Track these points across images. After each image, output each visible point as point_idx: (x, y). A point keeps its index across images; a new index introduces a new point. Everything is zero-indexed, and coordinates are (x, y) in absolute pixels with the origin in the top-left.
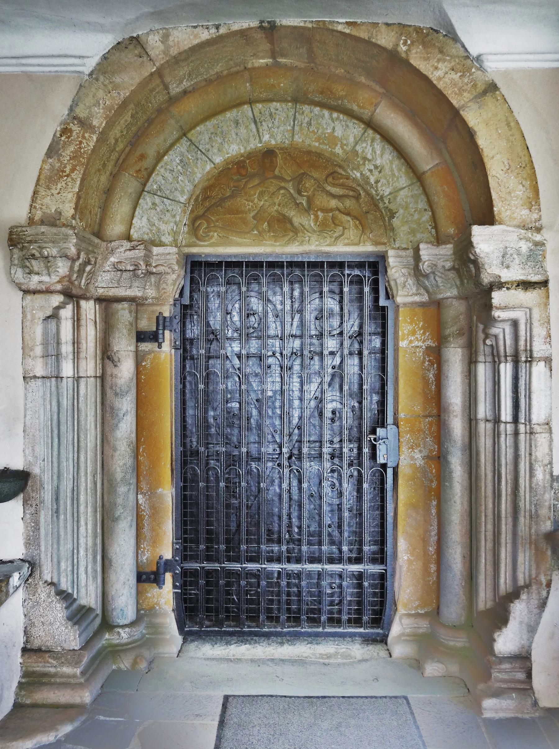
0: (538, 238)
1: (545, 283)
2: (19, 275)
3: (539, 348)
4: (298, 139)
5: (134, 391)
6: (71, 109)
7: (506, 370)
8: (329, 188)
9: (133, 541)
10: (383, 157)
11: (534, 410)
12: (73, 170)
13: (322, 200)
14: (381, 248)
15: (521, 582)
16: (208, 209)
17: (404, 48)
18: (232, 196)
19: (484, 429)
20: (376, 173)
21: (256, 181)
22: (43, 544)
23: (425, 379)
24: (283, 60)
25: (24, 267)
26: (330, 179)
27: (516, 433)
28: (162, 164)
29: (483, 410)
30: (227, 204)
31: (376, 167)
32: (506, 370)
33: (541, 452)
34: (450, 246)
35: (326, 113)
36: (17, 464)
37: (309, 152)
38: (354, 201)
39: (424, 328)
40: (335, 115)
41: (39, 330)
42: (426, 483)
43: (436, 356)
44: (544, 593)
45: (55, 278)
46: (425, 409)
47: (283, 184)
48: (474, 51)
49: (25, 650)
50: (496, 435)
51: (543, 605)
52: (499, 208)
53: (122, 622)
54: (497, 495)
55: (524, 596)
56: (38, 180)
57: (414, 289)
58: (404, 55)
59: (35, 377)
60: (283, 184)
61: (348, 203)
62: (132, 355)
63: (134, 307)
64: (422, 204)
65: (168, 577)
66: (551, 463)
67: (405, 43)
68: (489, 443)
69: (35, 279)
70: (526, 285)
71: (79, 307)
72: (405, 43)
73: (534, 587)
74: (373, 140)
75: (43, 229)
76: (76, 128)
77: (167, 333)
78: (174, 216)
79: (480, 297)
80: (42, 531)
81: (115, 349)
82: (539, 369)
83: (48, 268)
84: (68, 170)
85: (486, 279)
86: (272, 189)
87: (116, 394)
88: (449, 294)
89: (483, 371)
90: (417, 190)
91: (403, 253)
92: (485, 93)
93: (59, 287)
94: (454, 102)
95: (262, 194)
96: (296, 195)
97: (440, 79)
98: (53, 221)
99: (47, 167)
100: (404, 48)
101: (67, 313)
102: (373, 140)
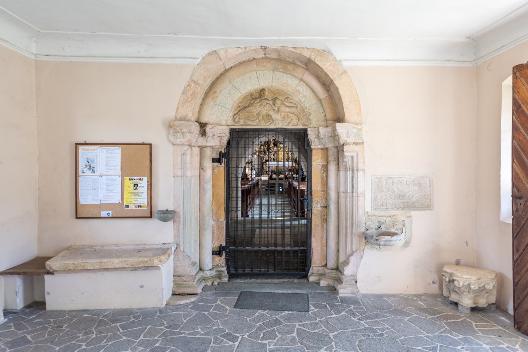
0: (360, 127)
1: (363, 143)
2: (172, 138)
3: (360, 166)
4: (274, 84)
5: (211, 182)
6: (191, 77)
7: (349, 174)
8: (286, 103)
9: (211, 238)
10: (307, 92)
11: (359, 188)
12: (192, 100)
13: (283, 109)
14: (305, 127)
15: (354, 250)
16: (239, 111)
17: (313, 57)
18: (249, 106)
19: (342, 195)
20: (304, 98)
21: (258, 101)
22: (181, 237)
23: (322, 177)
24: (269, 56)
25: (174, 136)
26: (286, 100)
27: (353, 197)
28: (221, 94)
29: (342, 189)
30: (247, 109)
31: (304, 96)
32: (349, 174)
33: (360, 204)
34: (331, 128)
35: (285, 75)
36: (171, 208)
37: (278, 90)
38: (295, 109)
39: (322, 158)
40: (288, 76)
41: (179, 159)
42: (322, 216)
43: (326, 168)
44: (362, 254)
45: (186, 140)
46: (322, 188)
47: (268, 102)
48: (338, 58)
49: (174, 276)
50: (346, 197)
51: (361, 258)
52: (347, 116)
53: (207, 269)
54: (347, 219)
55: (355, 254)
56: (179, 103)
57: (318, 143)
58: (313, 60)
59: (178, 176)
60: (268, 102)
61: (294, 110)
62: (211, 168)
63: (211, 149)
64: (321, 110)
65: (224, 252)
66: (364, 207)
67: (314, 55)
68: (344, 200)
69: (179, 140)
70: (356, 144)
71: (192, 149)
72: (314, 55)
73: (358, 251)
74: (303, 85)
75: (182, 122)
76: (193, 84)
77: (223, 159)
78: (226, 114)
79: (339, 149)
80: (181, 232)
81: (205, 165)
82: (360, 174)
83: (183, 136)
84: (190, 100)
85: (342, 142)
86: (264, 104)
87: (205, 183)
88: (330, 146)
89: (342, 174)
90: (319, 105)
91: (314, 129)
92: (342, 74)
93: (187, 143)
94: (331, 77)
95: (260, 106)
96: (273, 106)
97: (326, 68)
98: (184, 119)
99: (182, 98)
100: (313, 57)
101: (189, 152)
102: (303, 85)
